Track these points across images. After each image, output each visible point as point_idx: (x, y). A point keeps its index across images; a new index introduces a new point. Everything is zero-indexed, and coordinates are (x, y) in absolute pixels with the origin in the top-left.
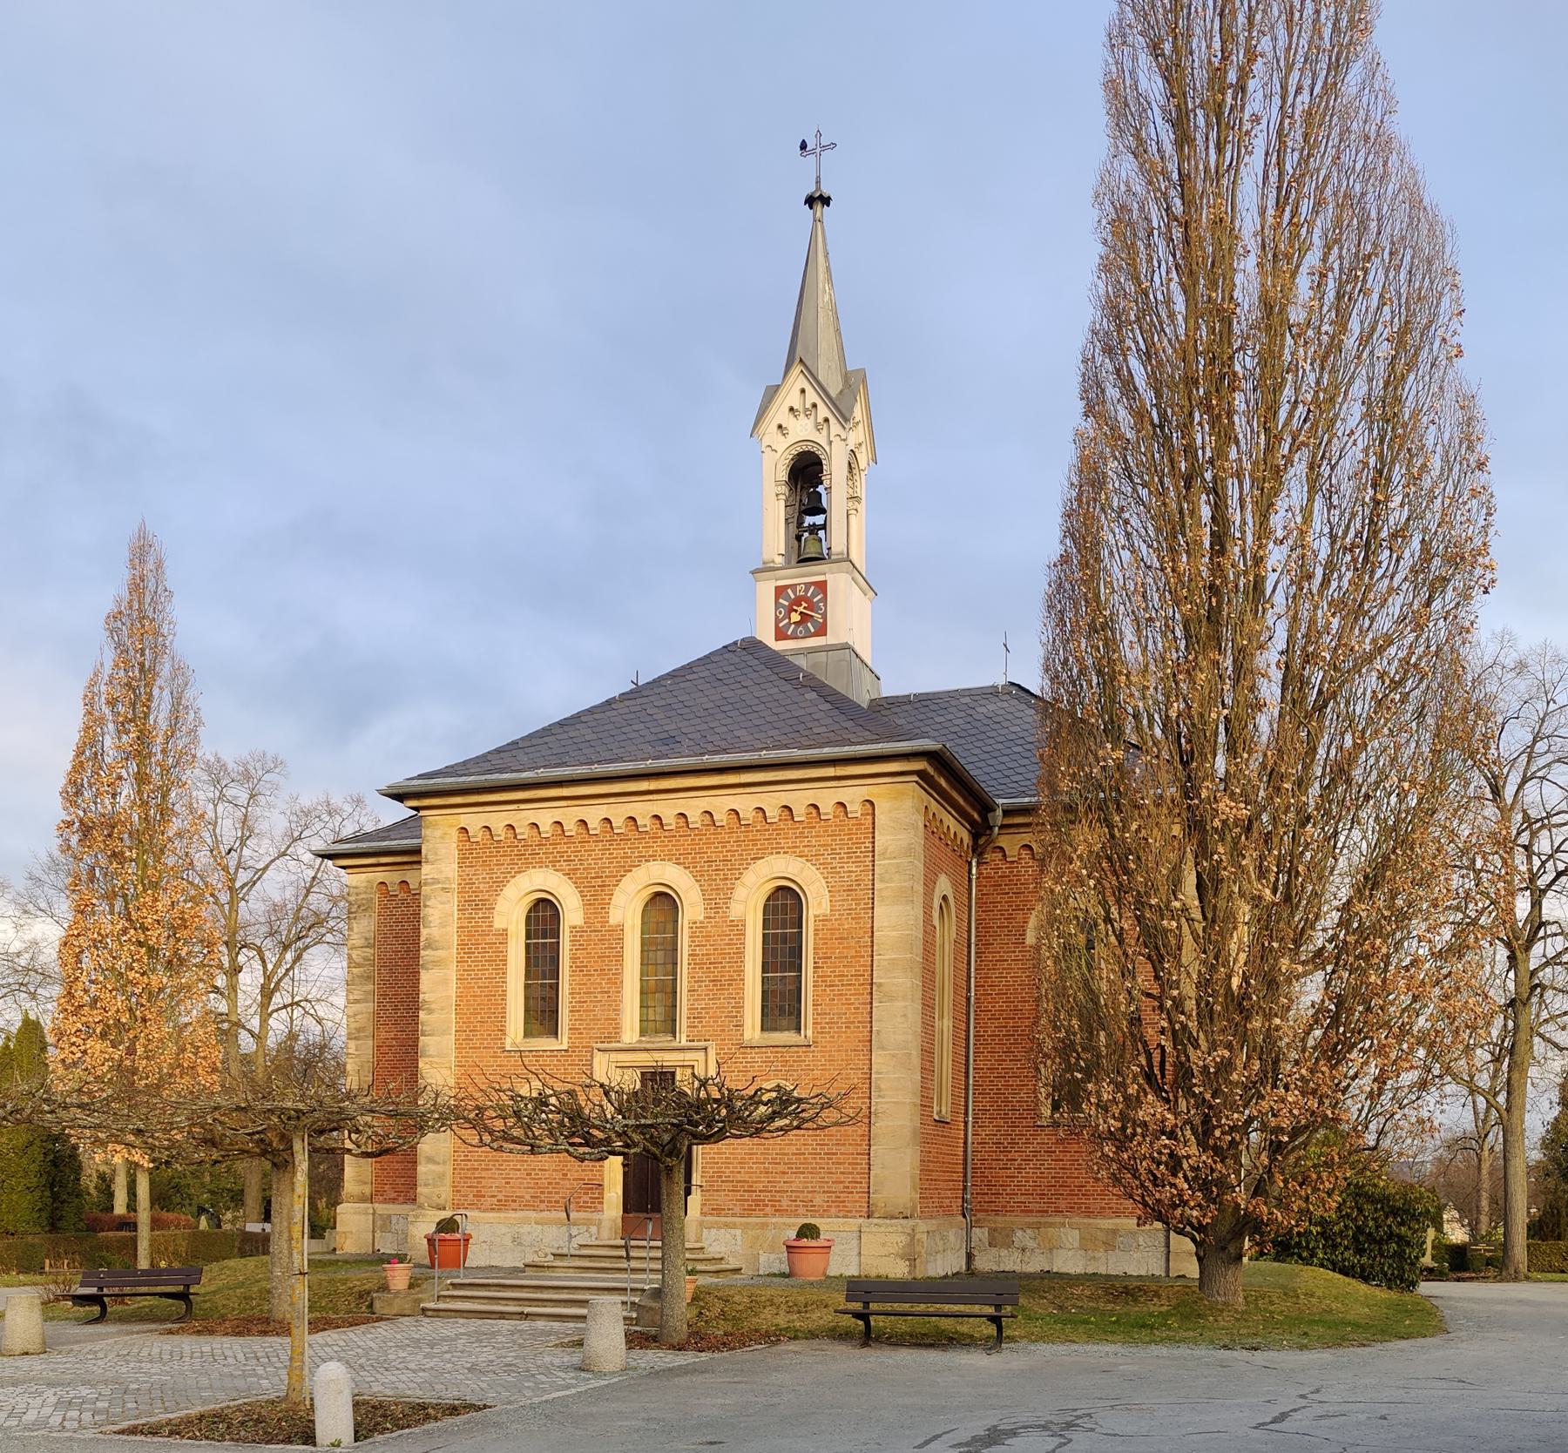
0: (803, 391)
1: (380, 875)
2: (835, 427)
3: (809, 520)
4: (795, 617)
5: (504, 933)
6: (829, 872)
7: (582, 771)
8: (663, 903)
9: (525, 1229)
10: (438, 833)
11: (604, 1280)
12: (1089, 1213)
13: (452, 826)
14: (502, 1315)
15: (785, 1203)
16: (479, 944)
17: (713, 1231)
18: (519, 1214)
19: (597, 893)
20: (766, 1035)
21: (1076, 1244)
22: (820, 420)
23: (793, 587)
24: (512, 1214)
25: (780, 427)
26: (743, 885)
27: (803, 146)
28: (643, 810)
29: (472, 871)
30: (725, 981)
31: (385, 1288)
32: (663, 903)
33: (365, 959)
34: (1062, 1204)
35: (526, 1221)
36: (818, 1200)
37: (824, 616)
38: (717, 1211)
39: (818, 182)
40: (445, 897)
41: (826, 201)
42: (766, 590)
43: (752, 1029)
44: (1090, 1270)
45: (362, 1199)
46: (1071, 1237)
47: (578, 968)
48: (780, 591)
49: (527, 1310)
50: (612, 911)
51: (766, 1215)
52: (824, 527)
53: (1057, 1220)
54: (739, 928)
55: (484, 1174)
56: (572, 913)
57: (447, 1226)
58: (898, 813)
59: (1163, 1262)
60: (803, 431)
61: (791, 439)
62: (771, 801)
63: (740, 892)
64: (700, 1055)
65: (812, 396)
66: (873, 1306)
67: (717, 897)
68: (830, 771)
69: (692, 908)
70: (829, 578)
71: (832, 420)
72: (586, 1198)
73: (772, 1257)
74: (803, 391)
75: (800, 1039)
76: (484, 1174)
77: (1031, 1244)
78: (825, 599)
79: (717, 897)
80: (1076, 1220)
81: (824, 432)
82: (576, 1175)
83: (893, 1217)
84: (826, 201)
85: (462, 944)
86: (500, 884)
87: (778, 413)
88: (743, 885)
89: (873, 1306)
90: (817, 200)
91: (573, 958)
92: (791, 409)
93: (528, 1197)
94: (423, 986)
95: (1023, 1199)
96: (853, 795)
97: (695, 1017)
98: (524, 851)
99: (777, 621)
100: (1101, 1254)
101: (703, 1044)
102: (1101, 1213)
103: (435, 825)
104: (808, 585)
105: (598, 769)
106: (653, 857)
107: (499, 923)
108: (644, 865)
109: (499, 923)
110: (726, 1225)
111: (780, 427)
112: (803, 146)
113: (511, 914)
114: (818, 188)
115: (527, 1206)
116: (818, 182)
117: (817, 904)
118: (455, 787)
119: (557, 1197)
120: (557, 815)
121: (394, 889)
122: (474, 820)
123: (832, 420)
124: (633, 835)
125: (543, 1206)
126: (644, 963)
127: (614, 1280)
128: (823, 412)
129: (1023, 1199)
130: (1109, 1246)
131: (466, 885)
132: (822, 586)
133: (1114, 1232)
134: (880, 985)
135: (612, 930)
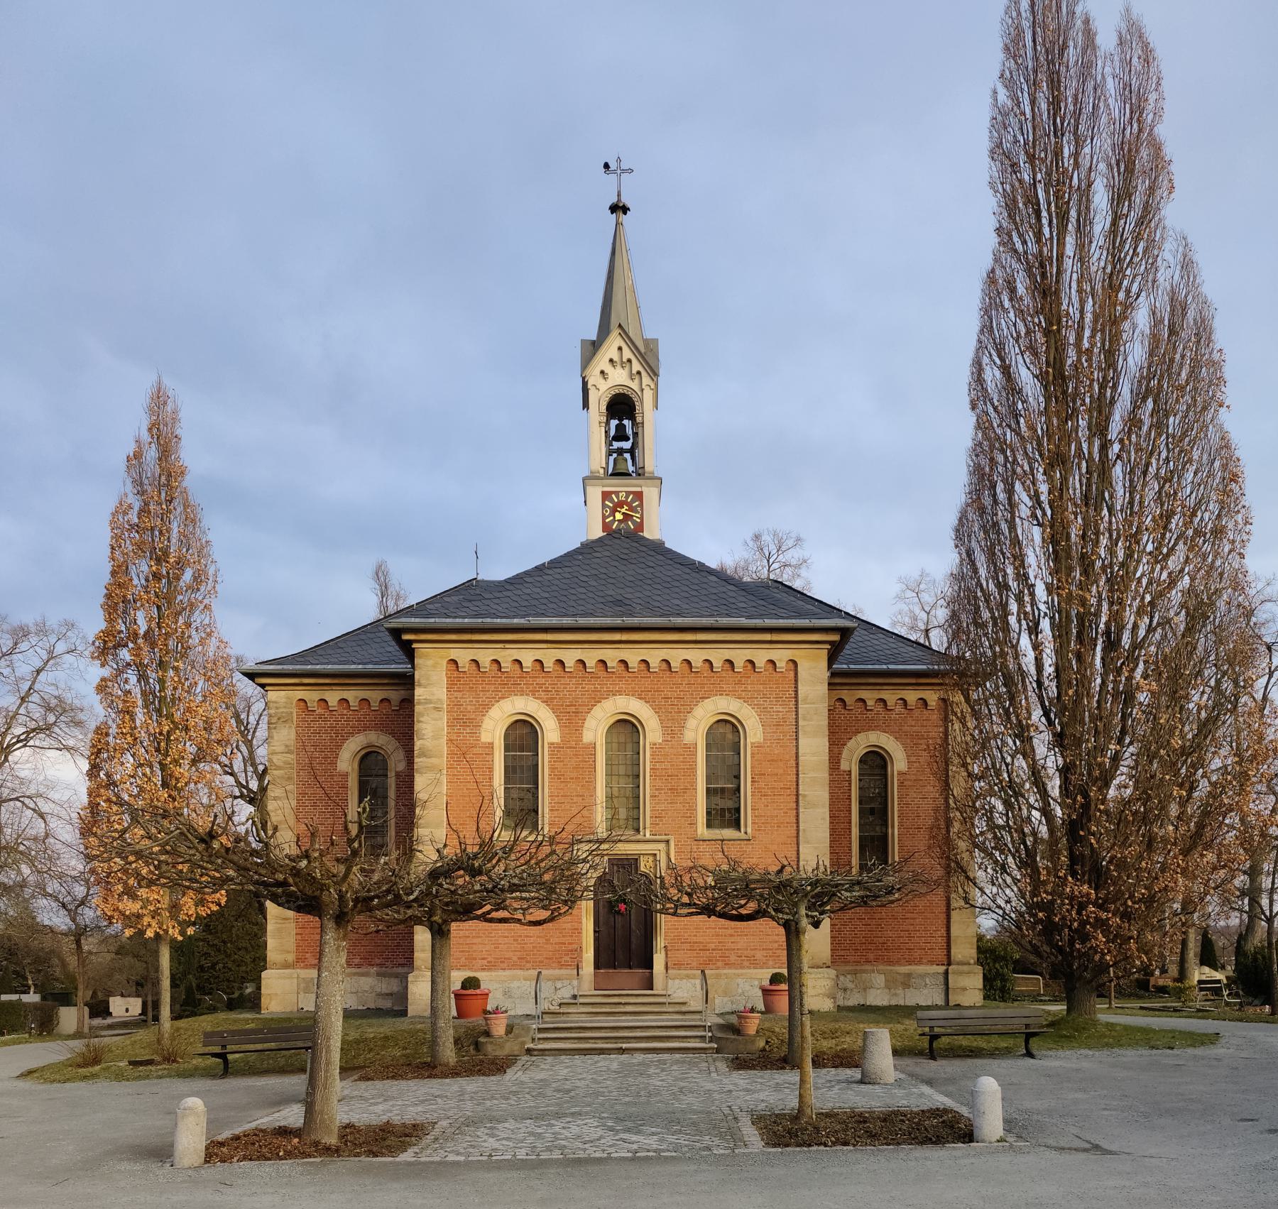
0: (620, 348)
1: (300, 694)
2: (646, 380)
3: (616, 445)
4: (619, 516)
5: (491, 746)
6: (762, 711)
7: (566, 621)
8: (627, 727)
9: (515, 984)
10: (430, 663)
11: (663, 1020)
12: (890, 963)
13: (442, 657)
14: (602, 1051)
15: (733, 958)
16: (465, 753)
17: (677, 981)
18: (508, 973)
19: (572, 718)
20: (711, 831)
21: (883, 985)
22: (634, 371)
23: (617, 493)
24: (501, 973)
25: (602, 372)
26: (694, 717)
27: (606, 166)
28: (612, 656)
29: (459, 695)
30: (678, 790)
31: (487, 1034)
32: (627, 727)
33: (285, 763)
34: (871, 956)
35: (514, 978)
36: (759, 955)
37: (642, 518)
38: (678, 965)
39: (619, 195)
40: (436, 714)
41: (625, 210)
42: (595, 493)
43: (702, 830)
44: (893, 1003)
45: (286, 966)
46: (879, 980)
47: (556, 775)
48: (606, 495)
49: (624, 1046)
50: (585, 732)
51: (718, 968)
52: (631, 452)
53: (868, 967)
54: (692, 749)
55: (475, 941)
56: (551, 731)
57: (470, 983)
58: (813, 669)
59: (943, 996)
60: (619, 378)
61: (610, 383)
62: (718, 656)
63: (691, 723)
64: (662, 846)
65: (627, 354)
66: (229, 1048)
67: (673, 727)
68: (768, 637)
69: (653, 732)
70: (645, 490)
71: (644, 374)
72: (567, 958)
73: (726, 999)
74: (620, 348)
75: (741, 835)
76: (475, 941)
77: (850, 985)
78: (641, 505)
79: (673, 727)
80: (881, 967)
81: (637, 381)
82: (557, 940)
83: (818, 967)
84: (625, 210)
85: (451, 754)
86: (486, 707)
87: (601, 362)
88: (694, 717)
89: (229, 1048)
90: (618, 208)
91: (552, 769)
92: (611, 360)
93: (515, 958)
94: (417, 787)
95: (842, 953)
96: (781, 655)
97: (657, 817)
98: (509, 680)
99: (604, 518)
100: (900, 991)
101: (664, 837)
102: (898, 963)
103: (426, 656)
104: (628, 493)
105: (725, 621)
106: (620, 692)
107: (485, 737)
108: (611, 699)
109: (485, 737)
110: (688, 977)
111: (602, 372)
112: (606, 166)
113: (494, 727)
114: (619, 200)
115: (513, 966)
116: (619, 195)
117: (754, 732)
118: (450, 626)
119: (541, 958)
120: (539, 655)
121: (313, 705)
122: (463, 655)
123: (644, 374)
124: (602, 674)
125: (528, 965)
126: (609, 774)
127: (668, 1020)
128: (636, 366)
129: (842, 953)
130: (906, 985)
131: (454, 706)
132: (639, 496)
133: (909, 975)
134: (805, 796)
135: (686, 746)
